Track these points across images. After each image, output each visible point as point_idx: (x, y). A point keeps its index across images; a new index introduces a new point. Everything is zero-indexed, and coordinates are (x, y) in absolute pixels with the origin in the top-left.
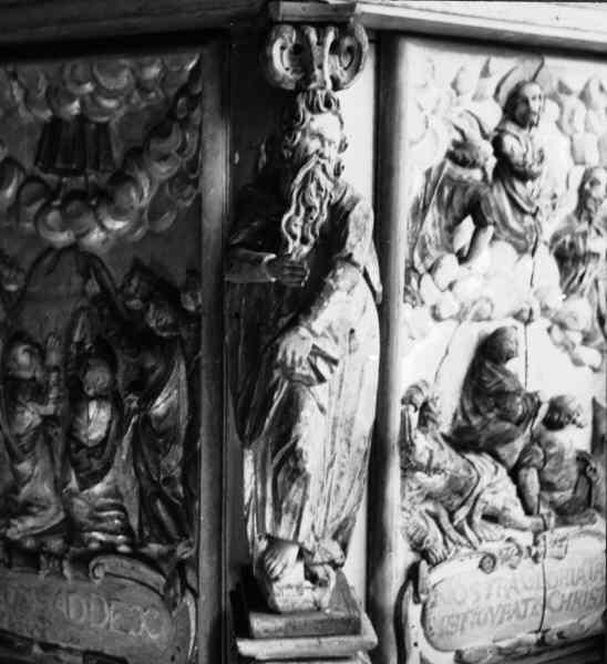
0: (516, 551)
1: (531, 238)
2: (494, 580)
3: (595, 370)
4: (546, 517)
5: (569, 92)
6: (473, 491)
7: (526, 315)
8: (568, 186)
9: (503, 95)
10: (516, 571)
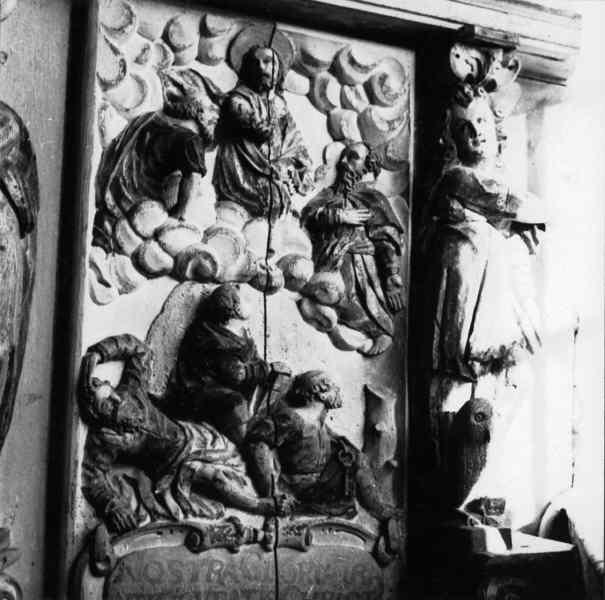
0: (233, 532)
1: (265, 200)
2: (204, 562)
3: (366, 356)
4: (278, 500)
5: (316, 63)
6: (176, 457)
7: (263, 281)
8: (325, 162)
9: (236, 59)
10: (235, 555)
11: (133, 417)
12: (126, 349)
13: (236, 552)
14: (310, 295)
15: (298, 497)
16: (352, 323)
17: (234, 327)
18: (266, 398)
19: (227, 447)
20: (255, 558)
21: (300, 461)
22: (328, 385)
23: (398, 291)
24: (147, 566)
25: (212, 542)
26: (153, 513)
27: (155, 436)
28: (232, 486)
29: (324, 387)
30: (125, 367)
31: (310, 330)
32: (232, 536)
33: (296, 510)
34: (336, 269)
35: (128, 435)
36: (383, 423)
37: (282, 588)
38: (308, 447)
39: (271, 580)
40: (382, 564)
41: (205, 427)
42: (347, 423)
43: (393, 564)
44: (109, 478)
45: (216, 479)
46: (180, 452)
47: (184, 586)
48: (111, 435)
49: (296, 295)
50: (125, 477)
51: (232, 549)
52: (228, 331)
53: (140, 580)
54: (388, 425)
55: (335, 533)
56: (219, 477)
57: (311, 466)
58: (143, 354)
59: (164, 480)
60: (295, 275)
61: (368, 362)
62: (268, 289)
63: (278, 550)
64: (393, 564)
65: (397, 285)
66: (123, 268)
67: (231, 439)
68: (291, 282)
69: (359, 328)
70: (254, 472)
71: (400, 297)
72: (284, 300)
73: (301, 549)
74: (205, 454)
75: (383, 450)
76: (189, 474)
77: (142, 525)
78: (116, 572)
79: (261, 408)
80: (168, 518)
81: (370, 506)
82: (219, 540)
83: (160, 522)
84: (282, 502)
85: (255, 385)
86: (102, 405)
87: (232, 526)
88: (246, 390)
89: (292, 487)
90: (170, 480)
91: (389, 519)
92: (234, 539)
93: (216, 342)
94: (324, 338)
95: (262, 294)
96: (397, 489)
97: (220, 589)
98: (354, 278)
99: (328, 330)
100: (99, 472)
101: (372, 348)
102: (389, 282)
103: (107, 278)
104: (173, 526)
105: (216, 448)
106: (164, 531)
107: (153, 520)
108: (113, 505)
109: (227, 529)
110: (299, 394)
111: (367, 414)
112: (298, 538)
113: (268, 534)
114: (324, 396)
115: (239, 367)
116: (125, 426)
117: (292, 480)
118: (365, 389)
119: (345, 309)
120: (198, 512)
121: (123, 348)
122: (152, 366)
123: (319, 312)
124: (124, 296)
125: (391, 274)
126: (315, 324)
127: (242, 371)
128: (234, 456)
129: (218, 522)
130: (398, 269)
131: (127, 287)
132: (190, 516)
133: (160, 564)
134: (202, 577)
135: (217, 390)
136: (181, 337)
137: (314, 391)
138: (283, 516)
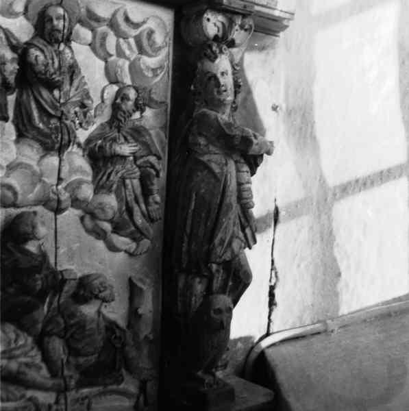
7: (54, 204)
14: (90, 213)
28: (32, 374)
31: (91, 239)
33: (80, 385)
34: (111, 192)
54: (147, 307)
68: (76, 202)
102: (151, 200)
123: (96, 225)
127: (39, 282)
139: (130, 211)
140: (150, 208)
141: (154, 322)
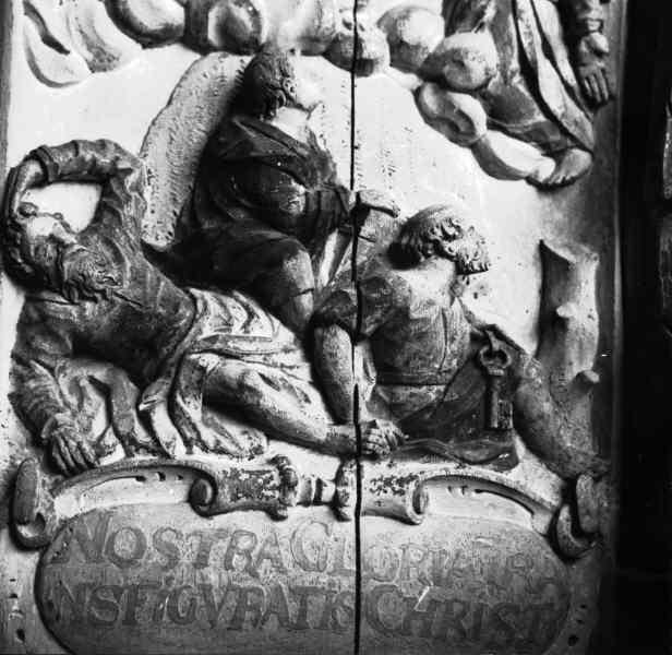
0: (276, 481)
2: (221, 533)
3: (545, 188)
6: (175, 348)
7: (349, 49)
10: (279, 525)
11: (96, 273)
12: (94, 161)
13: (283, 518)
14: (437, 74)
15: (404, 425)
16: (511, 126)
17: (288, 122)
18: (349, 251)
19: (276, 335)
20: (317, 532)
21: (407, 363)
22: (458, 228)
23: (601, 64)
24: (114, 535)
25: (235, 498)
26: (128, 442)
27: (138, 309)
28: (276, 401)
29: (451, 231)
30: (103, 195)
31: (437, 139)
32: (273, 488)
33: (399, 450)
34: (482, 26)
35: (88, 305)
36: (572, 305)
37: (369, 586)
38: (421, 336)
39: (346, 573)
40: (566, 556)
41: (237, 300)
42: (508, 303)
43: (588, 559)
44: (64, 382)
45: (242, 386)
46: (180, 341)
47: (182, 572)
48: (58, 306)
49: (412, 80)
50: (92, 380)
51: (274, 514)
52: (275, 129)
53: (98, 560)
54: (582, 310)
55: (474, 494)
56: (249, 382)
57: (427, 373)
58: (128, 171)
59: (155, 386)
60: (406, 39)
61: (547, 200)
62: (359, 66)
63: (362, 519)
64: (588, 559)
65: (599, 53)
66: (91, 24)
67: (285, 322)
68: (401, 53)
69: (527, 136)
70: (324, 380)
71: (606, 75)
72: (390, 87)
73: (408, 521)
74: (225, 341)
75: (572, 353)
76: (195, 376)
77: (106, 461)
78: (57, 545)
79: (340, 269)
80: (153, 453)
81: (543, 451)
82: (247, 496)
83: (140, 458)
84: (369, 433)
85: (331, 231)
86: (37, 249)
87: (275, 474)
88: (310, 233)
89: (392, 409)
90: (165, 388)
91: (578, 476)
92: (277, 494)
93: (247, 145)
94: (465, 156)
95: (349, 74)
96: (599, 426)
97: (251, 583)
98: (515, 43)
99: (471, 141)
100: (40, 369)
101: (552, 176)
102: (583, 48)
103: (58, 33)
104: (165, 467)
105: (252, 334)
106: (146, 474)
107: (129, 454)
108: (55, 426)
109: (268, 475)
110: (408, 245)
111: (544, 291)
112: (398, 499)
113: (340, 489)
114: (453, 247)
115: (293, 191)
116: (81, 289)
117: (392, 395)
118: (542, 247)
119: (498, 99)
120: (211, 445)
121: (88, 157)
122: (147, 195)
123: (450, 105)
124: (100, 75)
125: (588, 33)
126: (446, 127)
127: (301, 200)
128: (286, 351)
129: (256, 464)
130: (602, 22)
131: (101, 61)
132: (196, 449)
133: (138, 533)
134: (214, 559)
135: (254, 232)
136: (199, 148)
137: (432, 237)
138: (374, 457)
139: (529, 72)
140: (584, 71)
141: (605, 343)
